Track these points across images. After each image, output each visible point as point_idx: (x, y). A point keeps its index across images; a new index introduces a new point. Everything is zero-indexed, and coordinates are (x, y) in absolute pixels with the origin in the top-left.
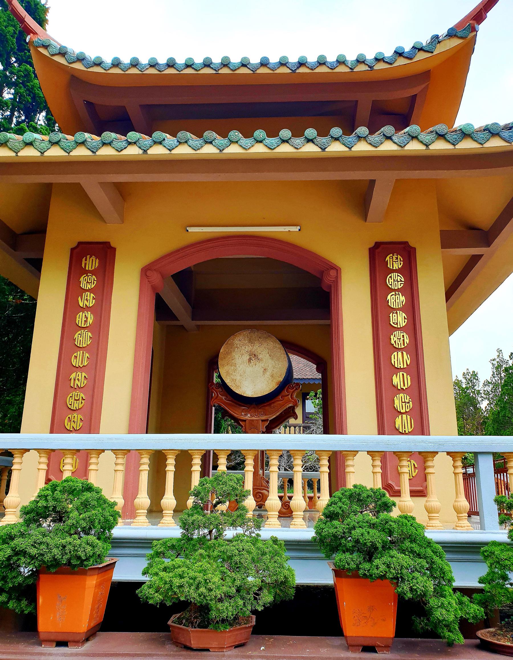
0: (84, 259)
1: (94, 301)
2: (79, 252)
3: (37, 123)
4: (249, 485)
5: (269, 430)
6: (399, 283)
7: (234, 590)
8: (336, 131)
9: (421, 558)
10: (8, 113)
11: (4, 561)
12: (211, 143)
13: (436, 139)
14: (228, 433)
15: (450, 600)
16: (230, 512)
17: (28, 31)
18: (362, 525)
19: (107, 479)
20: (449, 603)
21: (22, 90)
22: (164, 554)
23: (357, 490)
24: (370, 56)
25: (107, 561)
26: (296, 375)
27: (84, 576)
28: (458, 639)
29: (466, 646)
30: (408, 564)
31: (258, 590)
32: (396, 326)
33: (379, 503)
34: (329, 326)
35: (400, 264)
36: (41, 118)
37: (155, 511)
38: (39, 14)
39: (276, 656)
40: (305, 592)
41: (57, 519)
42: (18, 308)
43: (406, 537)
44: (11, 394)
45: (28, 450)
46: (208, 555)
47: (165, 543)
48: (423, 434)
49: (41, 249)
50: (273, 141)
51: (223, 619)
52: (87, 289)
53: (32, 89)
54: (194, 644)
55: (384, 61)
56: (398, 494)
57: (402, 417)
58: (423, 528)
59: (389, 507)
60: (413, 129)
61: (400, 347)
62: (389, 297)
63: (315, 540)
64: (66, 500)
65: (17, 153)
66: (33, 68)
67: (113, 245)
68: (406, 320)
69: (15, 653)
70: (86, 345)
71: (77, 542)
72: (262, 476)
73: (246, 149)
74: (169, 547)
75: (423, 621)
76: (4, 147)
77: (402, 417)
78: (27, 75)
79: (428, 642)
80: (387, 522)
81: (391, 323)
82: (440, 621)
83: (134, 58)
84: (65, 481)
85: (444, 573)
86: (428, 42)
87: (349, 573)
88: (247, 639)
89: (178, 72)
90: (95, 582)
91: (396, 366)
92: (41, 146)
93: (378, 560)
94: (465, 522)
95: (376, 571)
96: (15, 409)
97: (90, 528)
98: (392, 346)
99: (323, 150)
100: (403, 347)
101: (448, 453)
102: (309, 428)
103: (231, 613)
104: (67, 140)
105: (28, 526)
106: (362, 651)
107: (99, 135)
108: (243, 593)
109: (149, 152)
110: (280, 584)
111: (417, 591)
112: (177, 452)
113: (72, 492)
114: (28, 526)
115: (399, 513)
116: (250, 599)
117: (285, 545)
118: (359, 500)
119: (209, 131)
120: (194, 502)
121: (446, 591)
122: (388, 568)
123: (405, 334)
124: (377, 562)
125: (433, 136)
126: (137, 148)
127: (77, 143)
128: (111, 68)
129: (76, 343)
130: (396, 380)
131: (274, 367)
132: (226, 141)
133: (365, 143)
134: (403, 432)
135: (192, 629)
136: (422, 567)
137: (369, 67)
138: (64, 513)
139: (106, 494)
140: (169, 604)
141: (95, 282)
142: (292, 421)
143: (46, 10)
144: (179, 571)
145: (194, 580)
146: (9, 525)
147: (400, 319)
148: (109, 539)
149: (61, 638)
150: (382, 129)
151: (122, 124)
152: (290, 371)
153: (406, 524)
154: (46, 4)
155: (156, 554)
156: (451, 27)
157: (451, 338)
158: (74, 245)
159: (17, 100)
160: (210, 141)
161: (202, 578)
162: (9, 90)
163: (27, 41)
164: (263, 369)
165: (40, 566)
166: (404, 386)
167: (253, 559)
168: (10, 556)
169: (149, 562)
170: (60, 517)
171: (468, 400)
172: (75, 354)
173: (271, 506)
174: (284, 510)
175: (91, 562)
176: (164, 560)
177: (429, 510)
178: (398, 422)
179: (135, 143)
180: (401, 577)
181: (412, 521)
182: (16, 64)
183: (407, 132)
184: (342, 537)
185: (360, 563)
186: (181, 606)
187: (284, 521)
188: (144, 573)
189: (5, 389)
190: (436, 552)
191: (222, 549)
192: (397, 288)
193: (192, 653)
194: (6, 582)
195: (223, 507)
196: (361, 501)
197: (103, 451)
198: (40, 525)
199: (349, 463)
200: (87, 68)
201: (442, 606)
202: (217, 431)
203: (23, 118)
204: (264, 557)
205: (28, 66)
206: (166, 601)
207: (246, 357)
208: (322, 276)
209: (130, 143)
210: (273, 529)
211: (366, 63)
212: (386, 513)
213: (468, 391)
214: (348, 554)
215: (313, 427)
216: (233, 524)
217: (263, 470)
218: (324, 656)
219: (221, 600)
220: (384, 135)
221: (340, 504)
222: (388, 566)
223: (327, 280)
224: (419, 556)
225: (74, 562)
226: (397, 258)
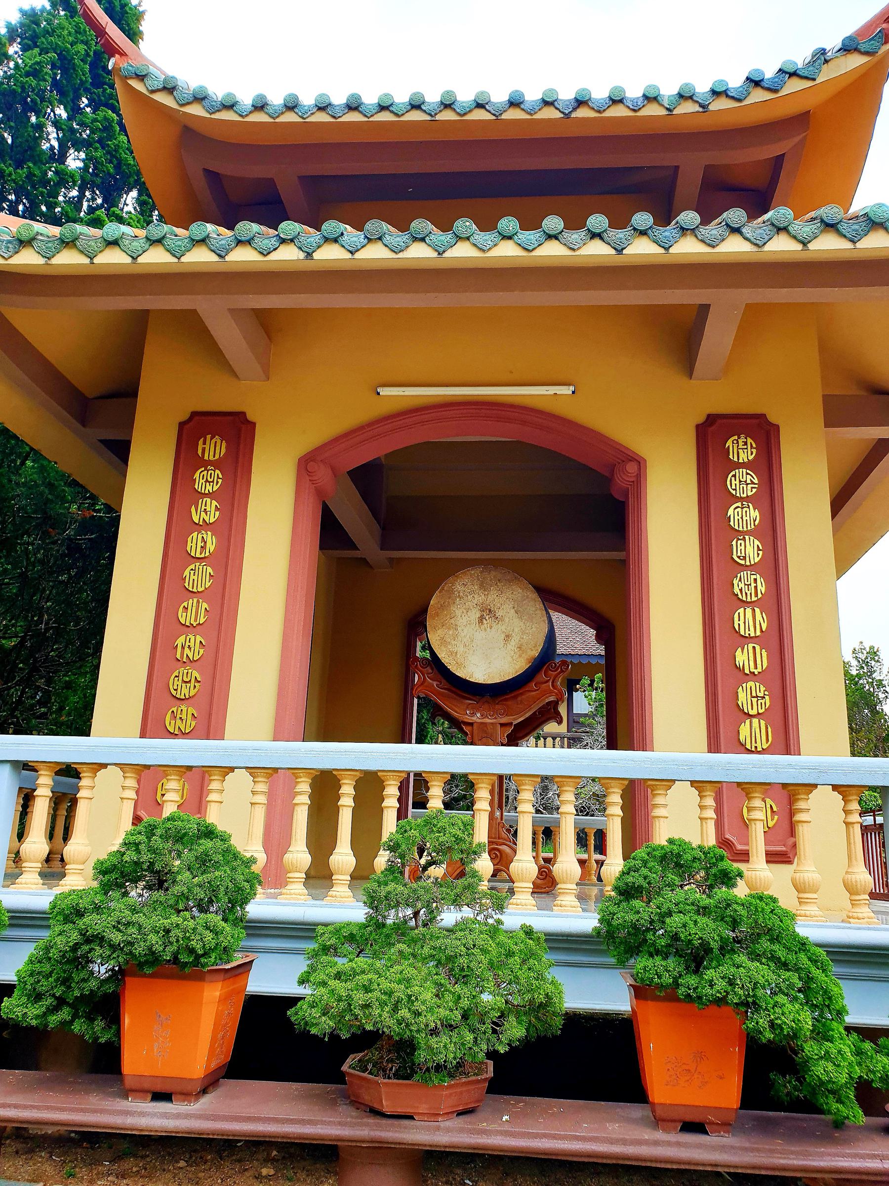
0: (201, 442)
1: (217, 513)
2: (194, 428)
3: (122, 210)
4: (481, 834)
5: (513, 740)
6: (750, 486)
7: (457, 1015)
8: (643, 219)
9: (789, 970)
10: (74, 193)
11: (66, 952)
12: (423, 240)
13: (822, 232)
14: (436, 743)
15: (842, 1046)
16: (449, 879)
17: (111, 49)
18: (683, 909)
19: (237, 816)
20: (839, 1052)
21: (99, 154)
22: (335, 949)
23: (675, 847)
24: (702, 88)
25: (238, 959)
26: (561, 649)
27: (202, 983)
28: (854, 1116)
29: (867, 1128)
30: (767, 981)
31: (500, 1017)
32: (742, 562)
33: (714, 871)
34: (624, 563)
35: (752, 454)
36: (130, 201)
37: (319, 876)
38: (128, 21)
39: (529, 1133)
40: (577, 1021)
41: (154, 885)
42: (86, 526)
43: (762, 932)
44: (70, 671)
45: (104, 766)
46: (412, 954)
47: (337, 931)
48: (788, 752)
49: (129, 424)
50: (531, 236)
51: (438, 1064)
52: (207, 492)
53: (115, 151)
54: (387, 1106)
55: (727, 96)
56: (744, 856)
57: (751, 723)
58: (793, 918)
59: (730, 879)
60: (779, 213)
61: (749, 600)
62: (731, 512)
63: (599, 933)
64: (170, 852)
65: (91, 259)
66: (119, 115)
67: (250, 417)
68: (761, 553)
69: (82, 1110)
70: (203, 588)
71: (190, 924)
72: (499, 820)
73: (484, 251)
74: (345, 937)
75: (790, 1082)
76: (71, 248)
77: (751, 723)
78: (107, 128)
79: (798, 1119)
80: (729, 905)
81: (735, 557)
82: (822, 1083)
83: (353, 95)
84: (168, 819)
85: (830, 998)
86: (806, 62)
87: (660, 991)
88: (478, 1101)
89: (366, 119)
90: (218, 994)
91: (742, 633)
92: (133, 246)
93: (712, 971)
94: (865, 911)
95: (708, 990)
96: (79, 697)
97: (211, 901)
98: (735, 598)
99: (620, 251)
100: (754, 599)
101: (835, 787)
102: (580, 740)
103: (452, 1055)
104: (176, 236)
105: (106, 894)
106: (680, 1130)
107: (231, 227)
108: (474, 1020)
109: (316, 256)
110: (538, 1007)
111: (782, 1029)
112: (357, 773)
113: (180, 838)
114: (106, 894)
115: (747, 891)
116: (484, 1033)
117: (546, 940)
118: (678, 865)
119: (420, 220)
120: (389, 860)
121: (833, 1030)
122: (731, 985)
123: (758, 576)
124: (710, 974)
125: (815, 226)
126: (296, 250)
127: (193, 240)
128: (251, 112)
129: (186, 585)
130: (741, 657)
131: (523, 633)
132: (450, 236)
133: (694, 239)
134: (753, 749)
135: (385, 1081)
136: (791, 986)
137: (701, 106)
138: (167, 873)
139: (238, 843)
140: (345, 1035)
141: (220, 481)
142: (551, 727)
143: (139, 16)
144: (363, 979)
145: (390, 996)
146: (74, 891)
147: (750, 550)
148: (242, 921)
149: (159, 1087)
150: (725, 215)
151: (269, 208)
152: (551, 639)
153: (763, 909)
154: (139, 5)
155: (323, 949)
156: (848, 35)
157: (845, 584)
158: (185, 416)
159: (91, 170)
160: (421, 236)
161: (402, 993)
162: (76, 153)
163: (110, 68)
164: (503, 636)
165: (127, 962)
166: (756, 668)
167: (491, 963)
168: (76, 944)
169: (309, 962)
170: (160, 881)
171: (861, 697)
172: (185, 604)
173: (520, 871)
174: (539, 881)
175: (212, 960)
176: (336, 959)
177: (800, 888)
178: (744, 731)
179: (292, 240)
180: (754, 1003)
181: (772, 904)
182: (88, 110)
183: (768, 220)
184: (648, 930)
185: (681, 975)
186: (366, 1040)
187: (545, 899)
188: (302, 982)
189: (62, 664)
190: (816, 961)
191: (438, 943)
192: (745, 495)
193: (384, 1121)
194: (69, 987)
195: (436, 872)
196: (681, 866)
197: (232, 769)
198: (126, 894)
199: (659, 800)
200: (211, 114)
201: (827, 1056)
202: (420, 740)
203: (99, 201)
204: (511, 960)
205: (110, 112)
206: (341, 1030)
207: (475, 614)
208: (613, 475)
209: (283, 241)
210: (522, 913)
211: (695, 98)
212: (724, 889)
213: (861, 682)
214: (658, 960)
215: (587, 739)
216: (457, 902)
217: (502, 809)
218: (614, 1136)
219: (434, 1032)
220: (727, 225)
221: (644, 871)
222: (731, 983)
223: (621, 480)
224: (785, 965)
225: (184, 958)
226: (746, 444)
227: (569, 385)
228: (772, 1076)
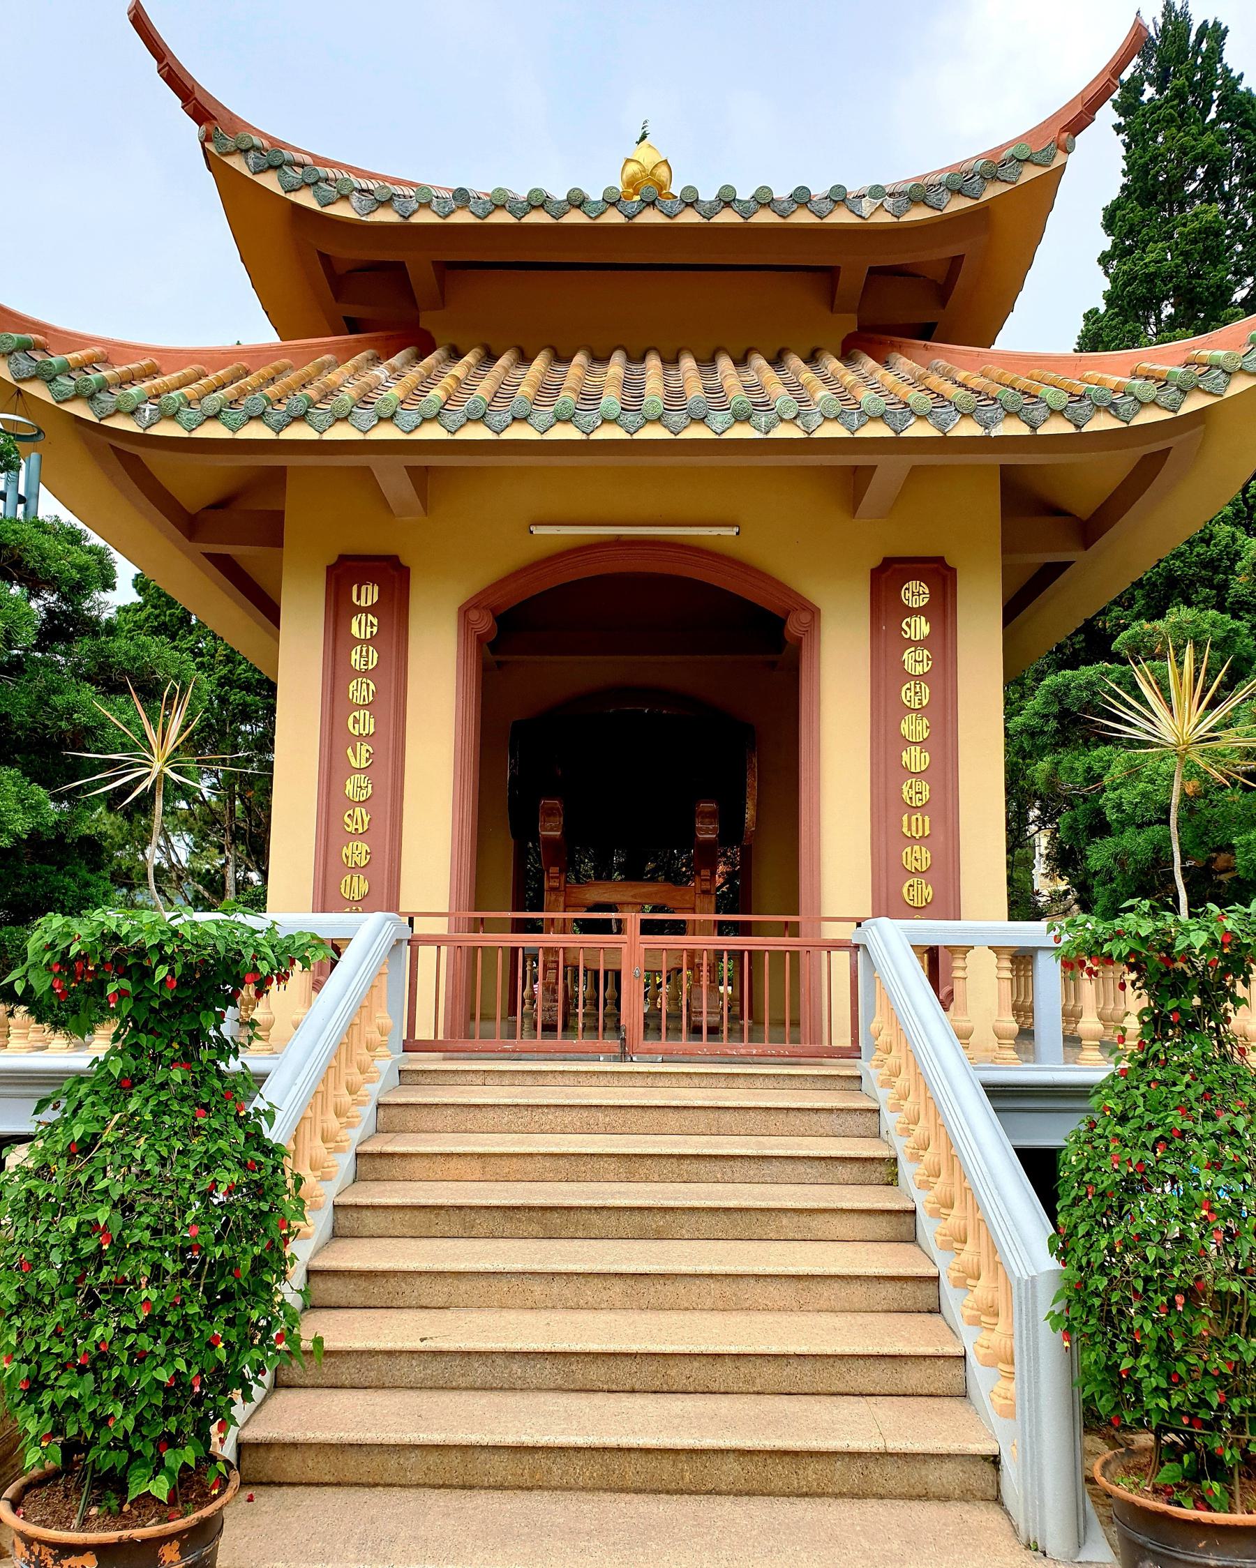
52: (368, 636)
62: (905, 656)
67: (405, 561)
223: (793, 627)
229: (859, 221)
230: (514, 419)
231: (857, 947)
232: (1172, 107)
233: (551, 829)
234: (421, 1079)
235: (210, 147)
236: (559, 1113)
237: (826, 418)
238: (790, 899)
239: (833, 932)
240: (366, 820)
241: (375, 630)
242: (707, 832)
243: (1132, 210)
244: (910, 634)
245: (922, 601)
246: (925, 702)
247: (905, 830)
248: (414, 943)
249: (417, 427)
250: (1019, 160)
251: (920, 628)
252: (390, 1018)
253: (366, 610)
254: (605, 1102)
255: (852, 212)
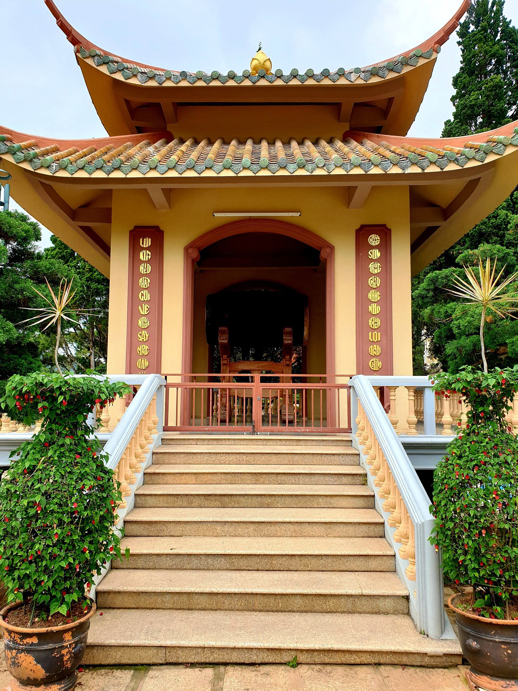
52: (147, 260)
62: (370, 266)
67: (161, 228)
200: (17, 163)
223: (323, 254)
227: (298, 212)
228: (479, 646)
229: (350, 83)
230: (206, 168)
231: (350, 387)
232: (481, 34)
233: (223, 340)
234: (170, 442)
235: (79, 55)
236: (227, 456)
237: (336, 166)
238: (322, 367)
239: (340, 381)
240: (147, 336)
241: (150, 257)
242: (288, 340)
243: (465, 78)
244: (372, 257)
245: (377, 243)
246: (378, 285)
247: (370, 338)
248: (167, 386)
249: (166, 172)
250: (417, 56)
251: (376, 254)
252: (157, 418)
253: (146, 249)
254: (246, 451)
255: (347, 79)
